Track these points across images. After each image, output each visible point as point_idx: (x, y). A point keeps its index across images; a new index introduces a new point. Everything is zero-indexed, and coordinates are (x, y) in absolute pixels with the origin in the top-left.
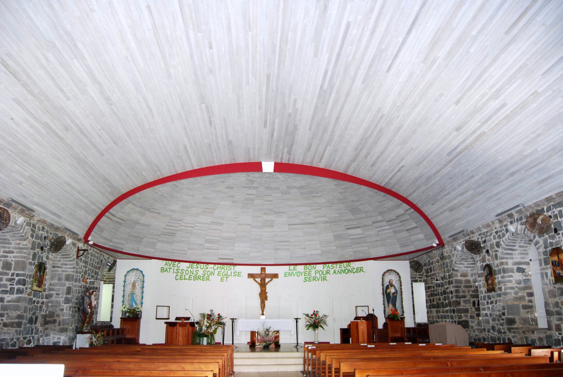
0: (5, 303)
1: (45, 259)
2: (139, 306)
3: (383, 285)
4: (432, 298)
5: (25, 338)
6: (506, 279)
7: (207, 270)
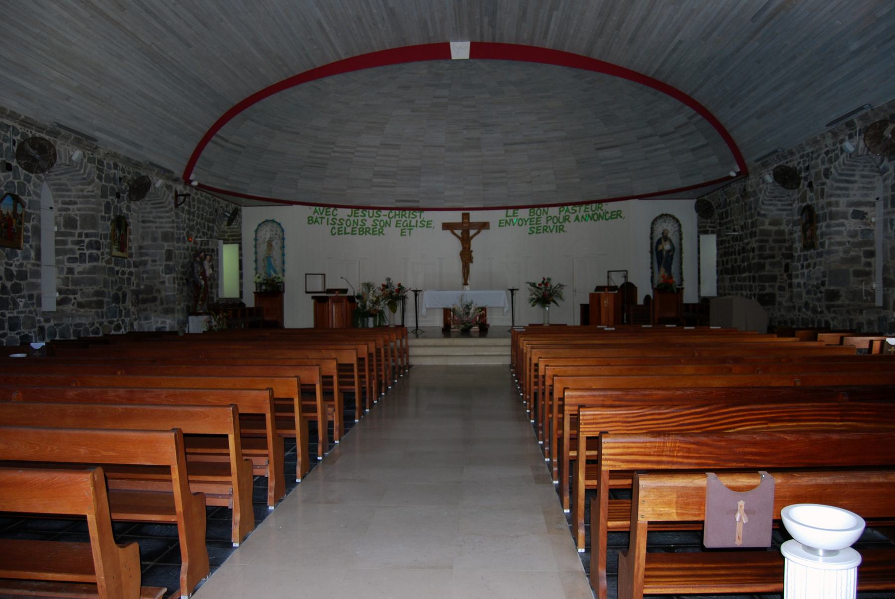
0: (76, 275)
1: (125, 211)
2: (280, 275)
3: (652, 238)
4: (725, 259)
5: (111, 323)
6: (833, 229)
7: (379, 219)
